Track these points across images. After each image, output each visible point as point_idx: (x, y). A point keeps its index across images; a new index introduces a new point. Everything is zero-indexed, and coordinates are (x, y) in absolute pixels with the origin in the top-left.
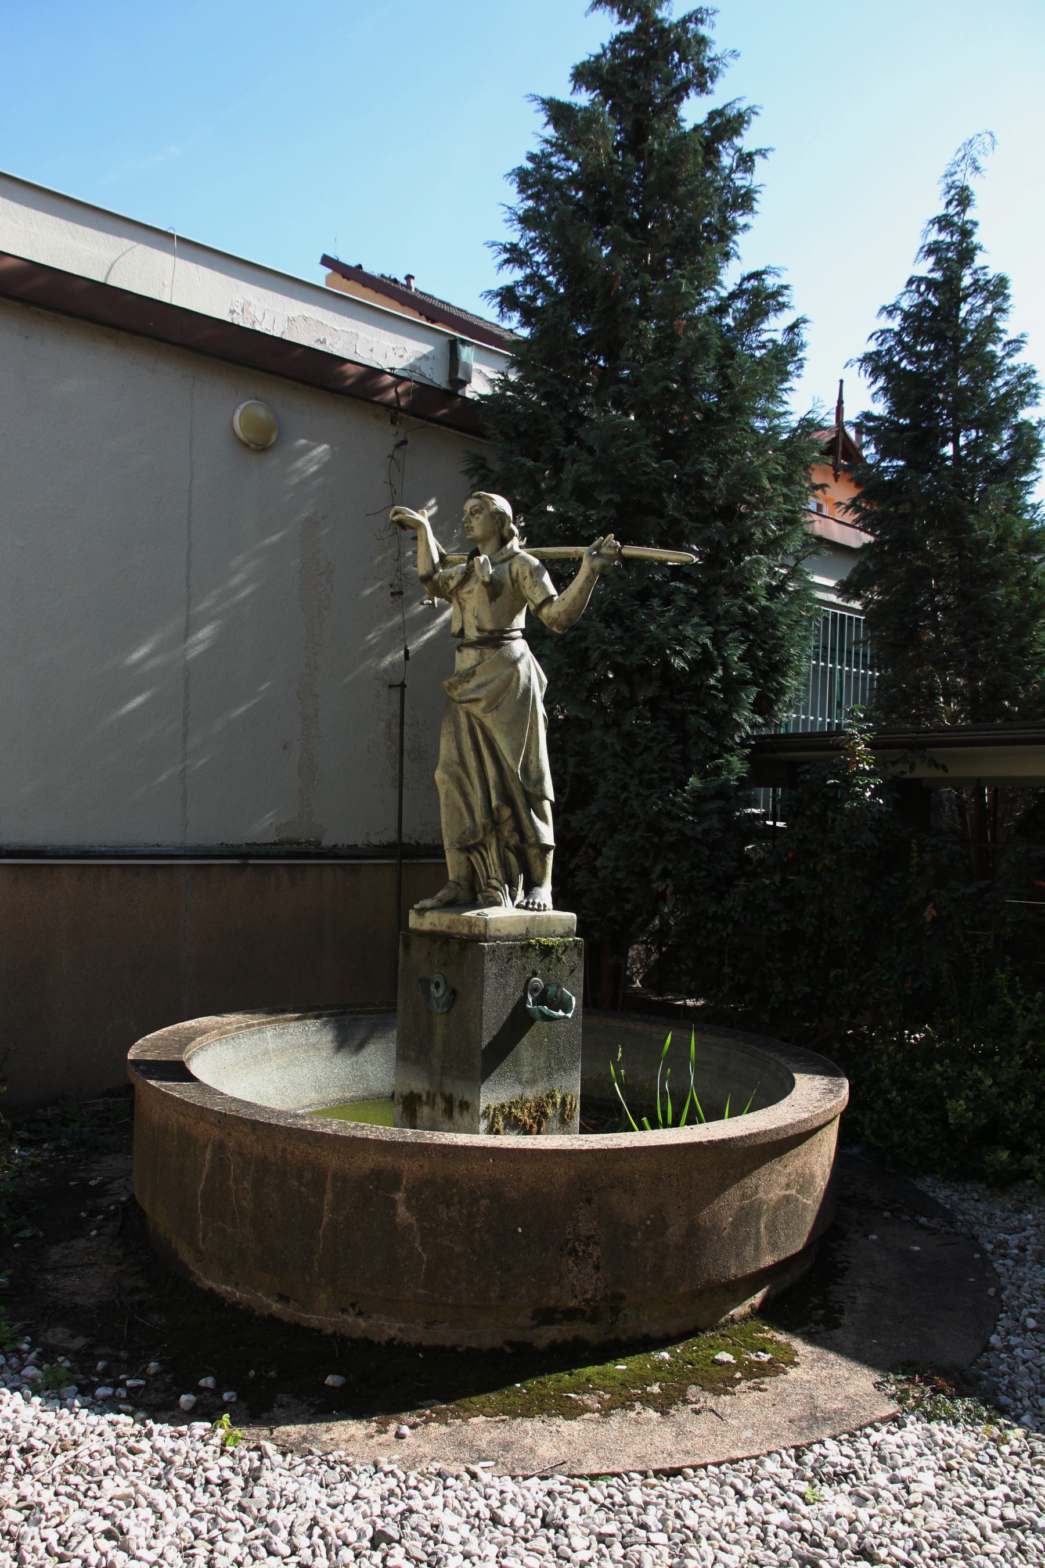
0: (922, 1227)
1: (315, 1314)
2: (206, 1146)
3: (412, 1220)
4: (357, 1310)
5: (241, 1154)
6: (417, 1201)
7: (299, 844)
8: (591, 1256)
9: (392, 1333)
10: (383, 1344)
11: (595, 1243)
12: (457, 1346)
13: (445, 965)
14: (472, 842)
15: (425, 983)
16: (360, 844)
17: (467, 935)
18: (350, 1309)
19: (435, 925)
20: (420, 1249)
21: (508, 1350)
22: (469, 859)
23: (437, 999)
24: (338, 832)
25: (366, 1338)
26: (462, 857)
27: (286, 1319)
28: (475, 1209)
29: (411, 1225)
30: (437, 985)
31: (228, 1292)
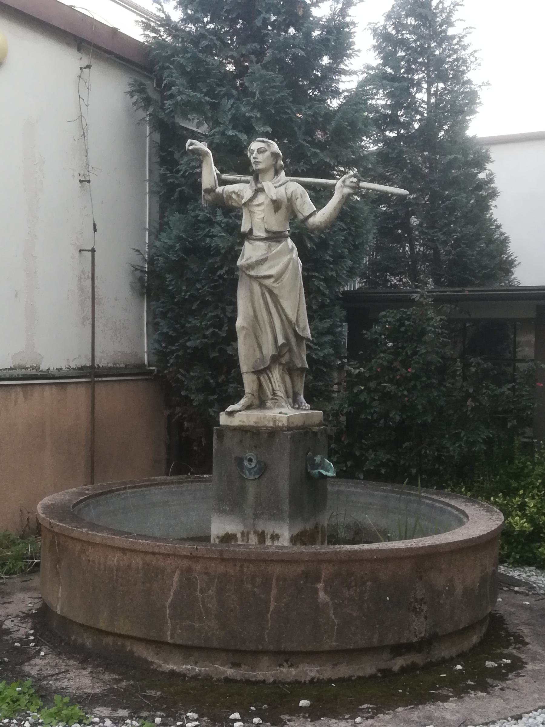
0: (517, 592)
1: (260, 671)
2: (174, 572)
3: (328, 600)
4: (289, 663)
5: (207, 574)
6: (331, 587)
7: (26, 368)
8: (422, 610)
9: (313, 674)
10: (307, 682)
11: (425, 603)
12: (352, 676)
13: (256, 447)
14: (262, 367)
15: (239, 461)
16: (64, 368)
17: (271, 427)
18: (285, 664)
19: (244, 422)
20: (333, 617)
21: (379, 675)
22: (259, 379)
23: (249, 470)
24: (50, 363)
25: (296, 680)
26: (255, 377)
27: (238, 678)
28: (364, 589)
29: (327, 603)
30: (250, 460)
31: (189, 670)
